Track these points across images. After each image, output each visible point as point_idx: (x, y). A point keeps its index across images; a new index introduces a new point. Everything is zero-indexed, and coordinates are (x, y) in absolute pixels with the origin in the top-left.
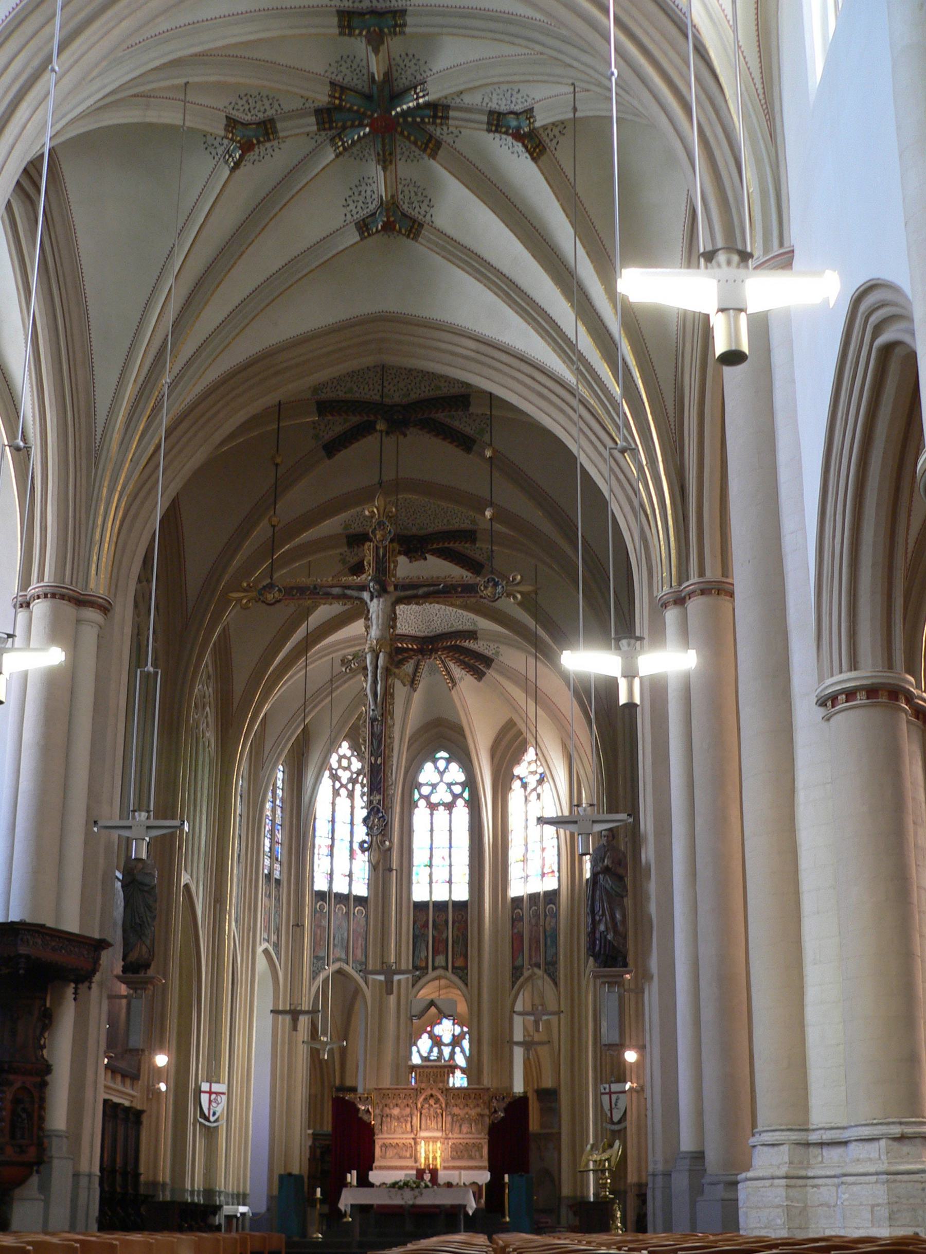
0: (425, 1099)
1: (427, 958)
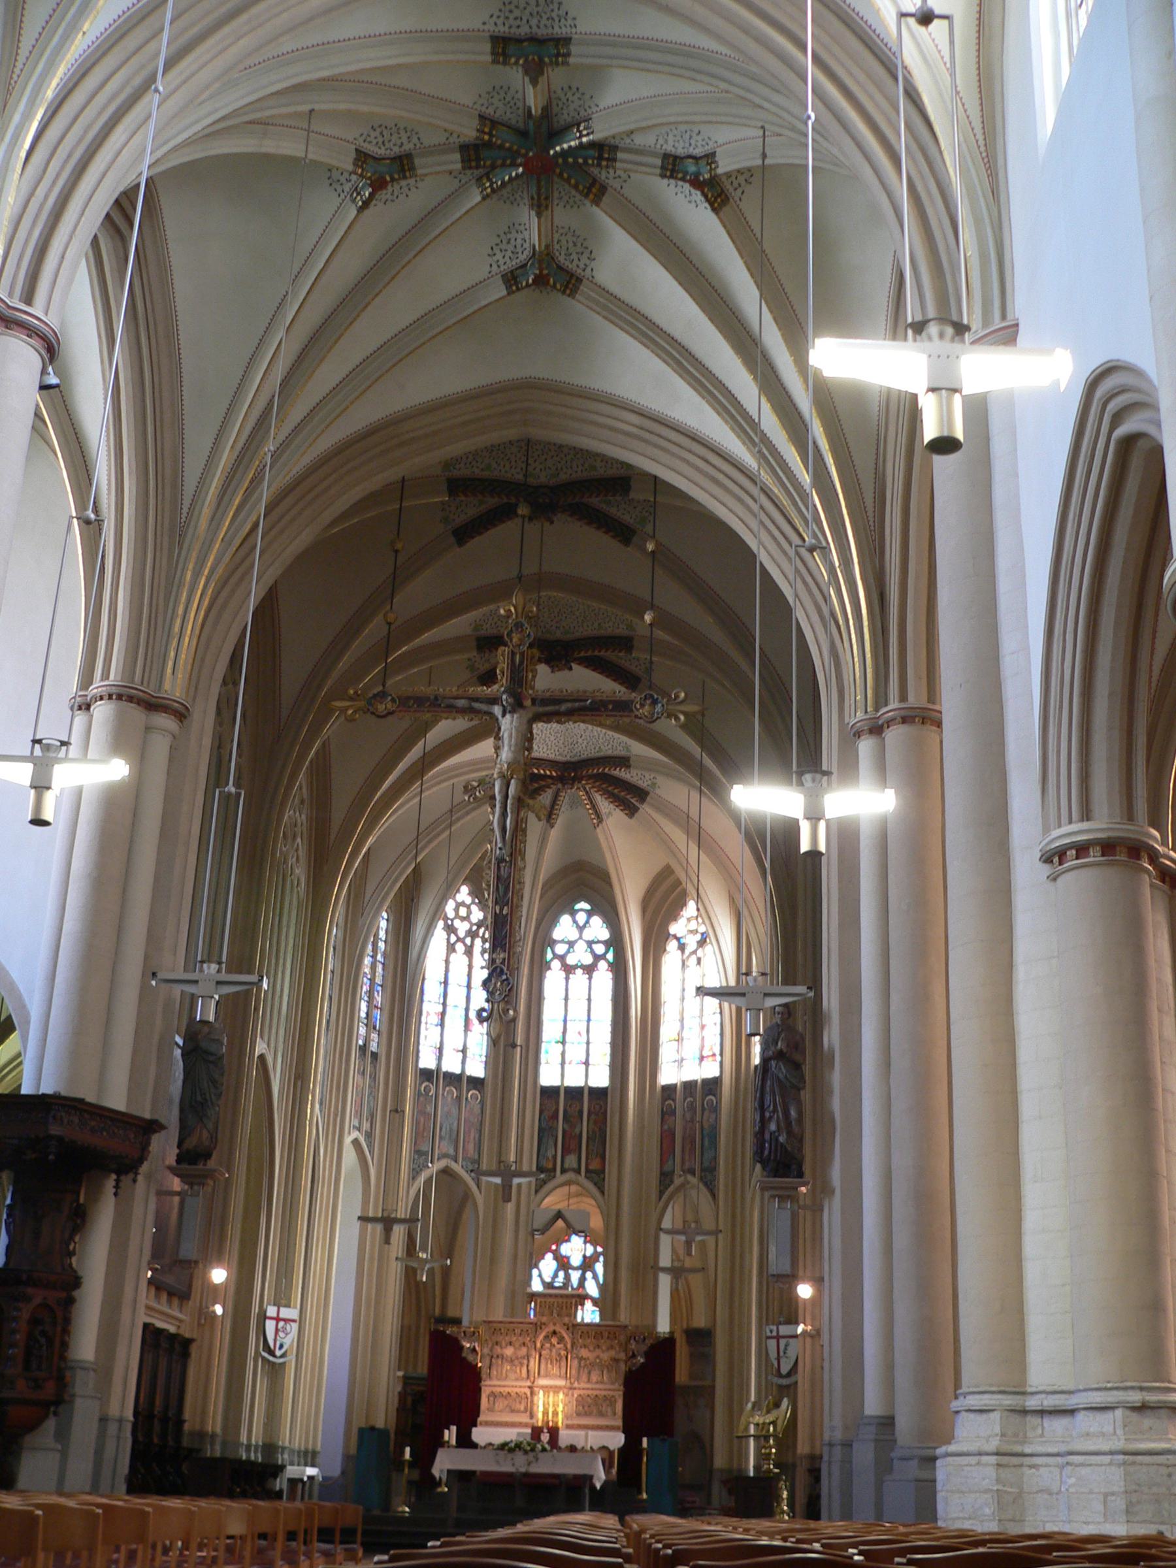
0: (546, 1337)
1: (555, 1157)
